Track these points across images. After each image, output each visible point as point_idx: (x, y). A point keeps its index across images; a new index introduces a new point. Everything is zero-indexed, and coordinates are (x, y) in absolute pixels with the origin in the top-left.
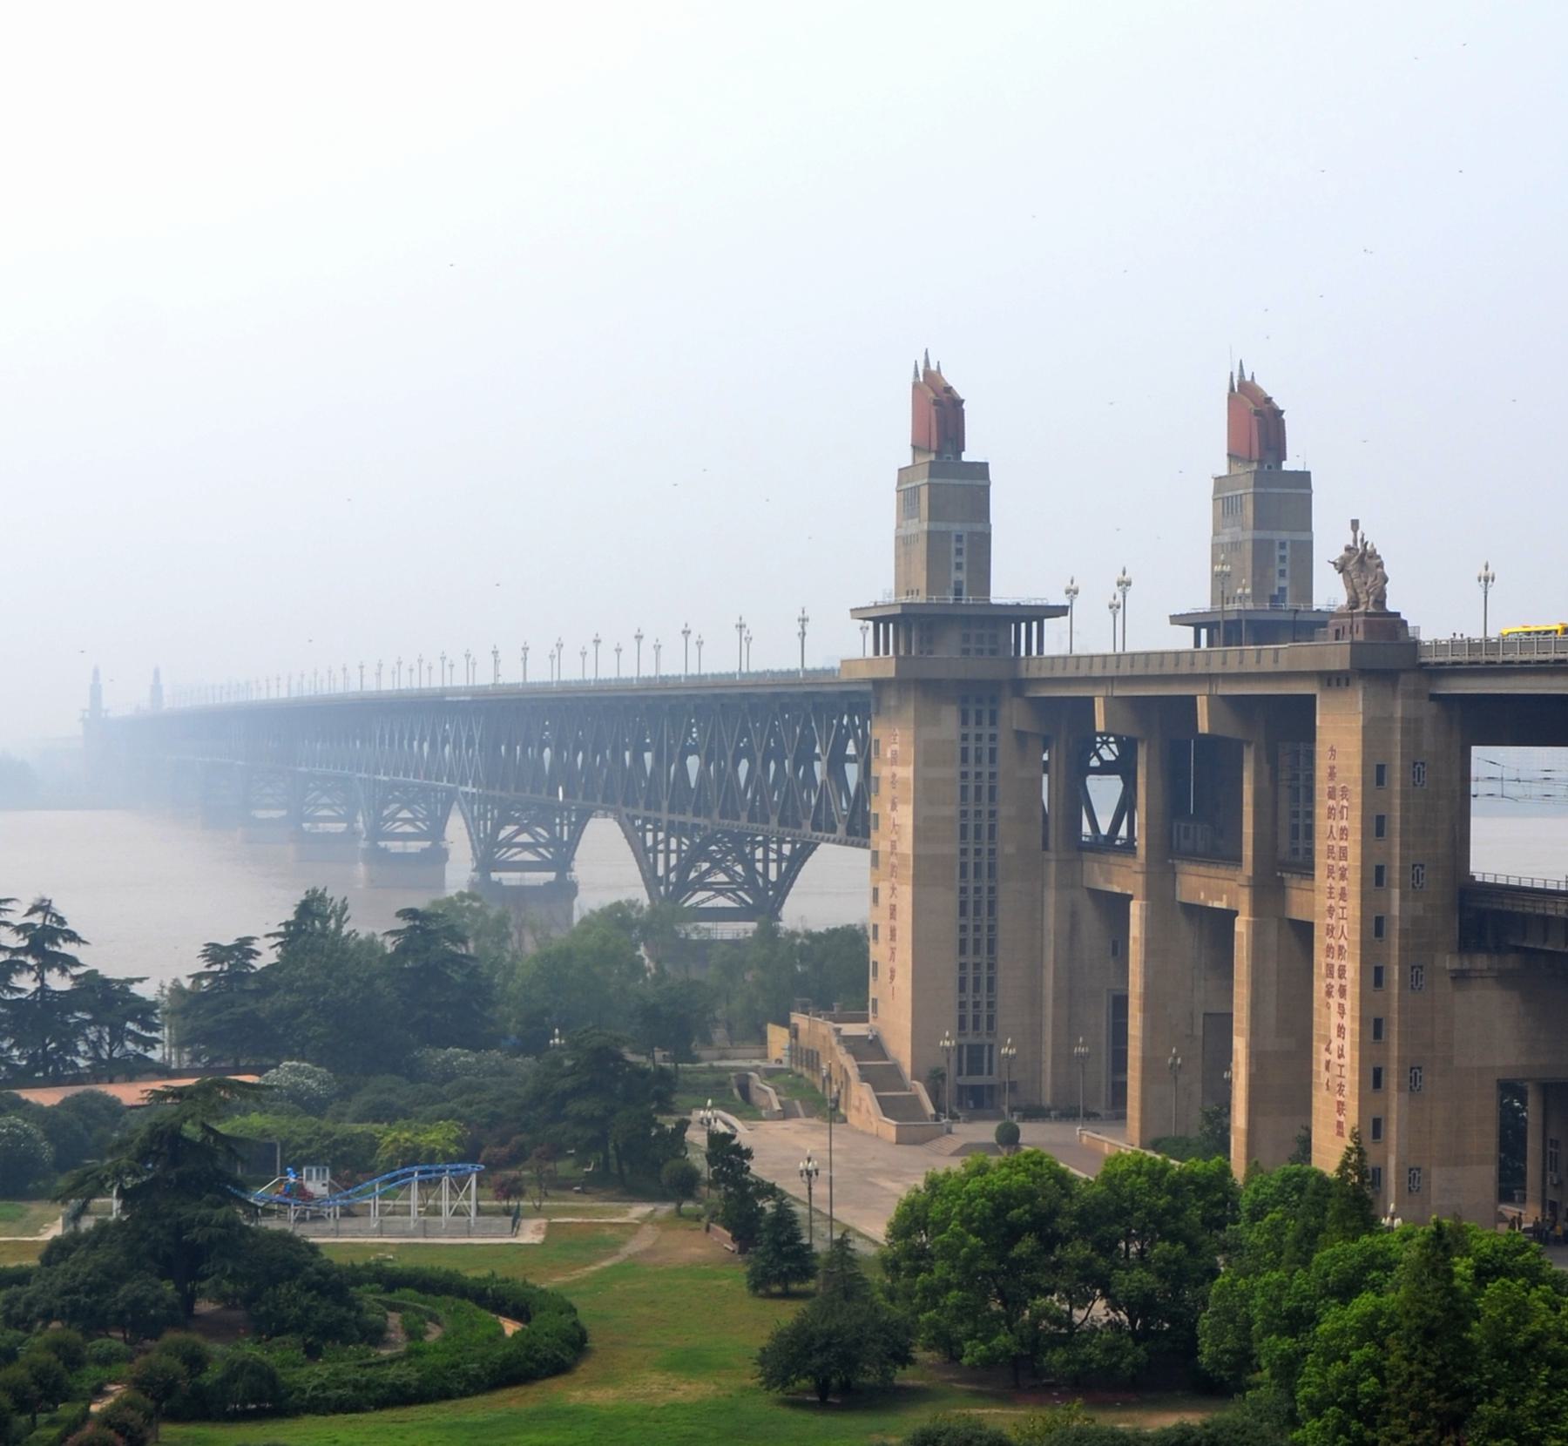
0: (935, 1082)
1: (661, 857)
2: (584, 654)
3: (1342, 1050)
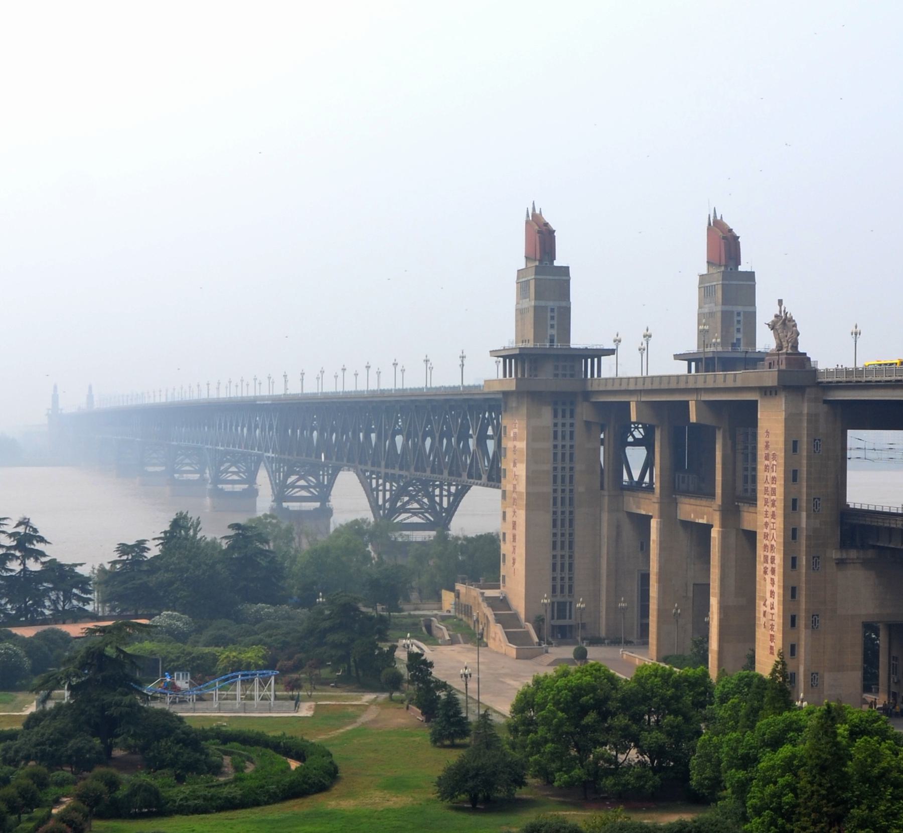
0: (538, 623)
1: (381, 494)
2: (336, 377)
3: (773, 605)
